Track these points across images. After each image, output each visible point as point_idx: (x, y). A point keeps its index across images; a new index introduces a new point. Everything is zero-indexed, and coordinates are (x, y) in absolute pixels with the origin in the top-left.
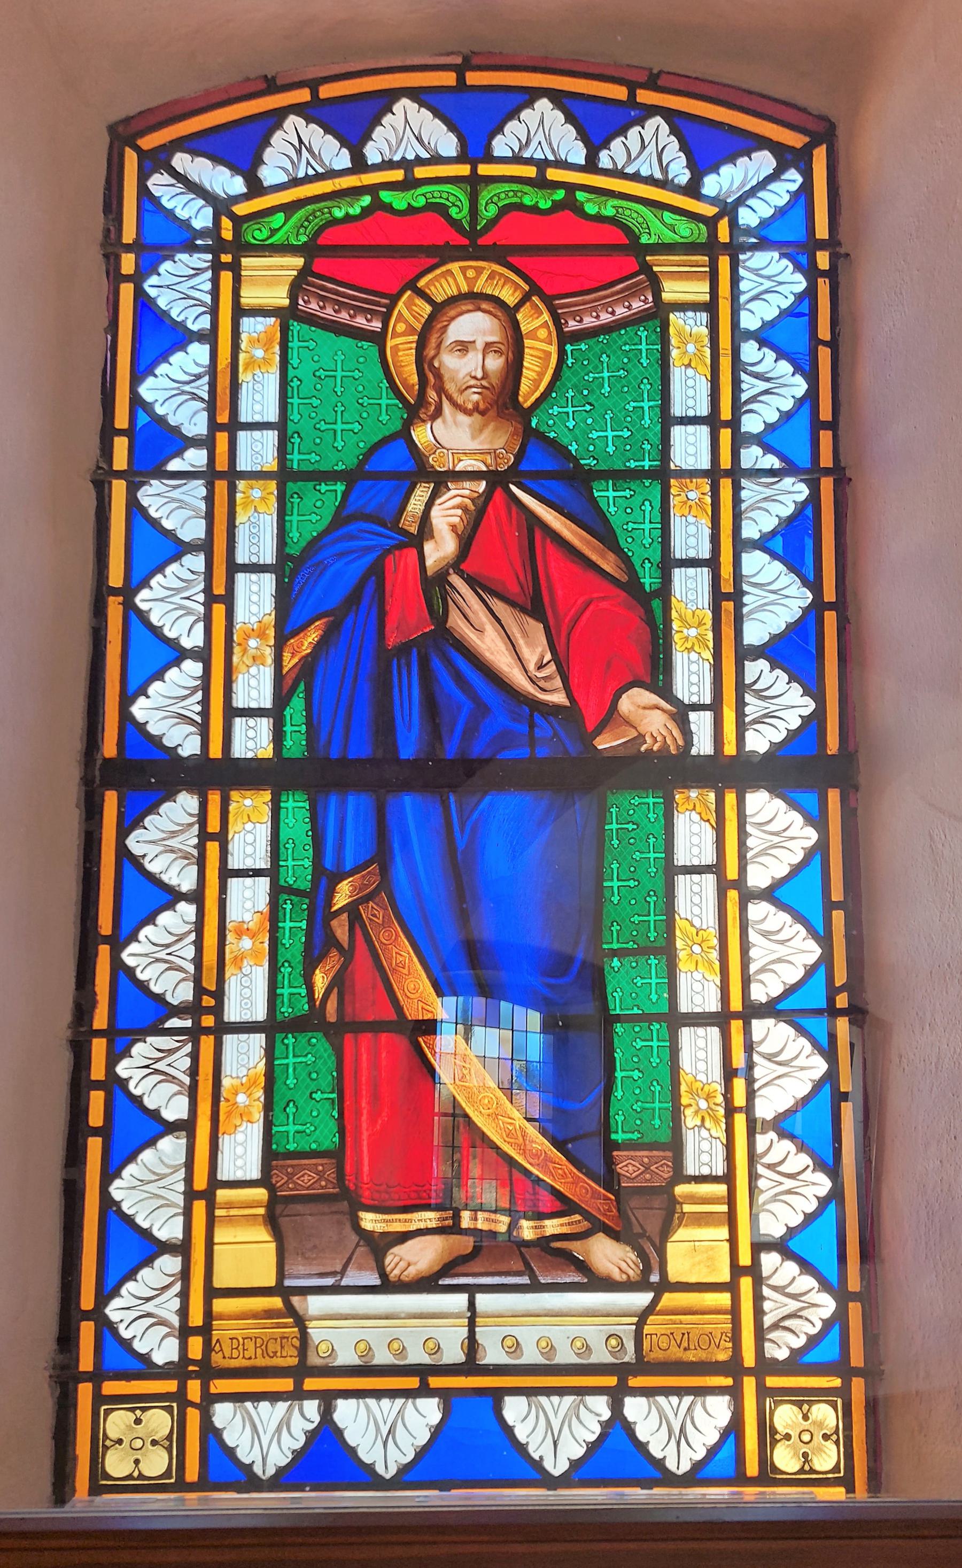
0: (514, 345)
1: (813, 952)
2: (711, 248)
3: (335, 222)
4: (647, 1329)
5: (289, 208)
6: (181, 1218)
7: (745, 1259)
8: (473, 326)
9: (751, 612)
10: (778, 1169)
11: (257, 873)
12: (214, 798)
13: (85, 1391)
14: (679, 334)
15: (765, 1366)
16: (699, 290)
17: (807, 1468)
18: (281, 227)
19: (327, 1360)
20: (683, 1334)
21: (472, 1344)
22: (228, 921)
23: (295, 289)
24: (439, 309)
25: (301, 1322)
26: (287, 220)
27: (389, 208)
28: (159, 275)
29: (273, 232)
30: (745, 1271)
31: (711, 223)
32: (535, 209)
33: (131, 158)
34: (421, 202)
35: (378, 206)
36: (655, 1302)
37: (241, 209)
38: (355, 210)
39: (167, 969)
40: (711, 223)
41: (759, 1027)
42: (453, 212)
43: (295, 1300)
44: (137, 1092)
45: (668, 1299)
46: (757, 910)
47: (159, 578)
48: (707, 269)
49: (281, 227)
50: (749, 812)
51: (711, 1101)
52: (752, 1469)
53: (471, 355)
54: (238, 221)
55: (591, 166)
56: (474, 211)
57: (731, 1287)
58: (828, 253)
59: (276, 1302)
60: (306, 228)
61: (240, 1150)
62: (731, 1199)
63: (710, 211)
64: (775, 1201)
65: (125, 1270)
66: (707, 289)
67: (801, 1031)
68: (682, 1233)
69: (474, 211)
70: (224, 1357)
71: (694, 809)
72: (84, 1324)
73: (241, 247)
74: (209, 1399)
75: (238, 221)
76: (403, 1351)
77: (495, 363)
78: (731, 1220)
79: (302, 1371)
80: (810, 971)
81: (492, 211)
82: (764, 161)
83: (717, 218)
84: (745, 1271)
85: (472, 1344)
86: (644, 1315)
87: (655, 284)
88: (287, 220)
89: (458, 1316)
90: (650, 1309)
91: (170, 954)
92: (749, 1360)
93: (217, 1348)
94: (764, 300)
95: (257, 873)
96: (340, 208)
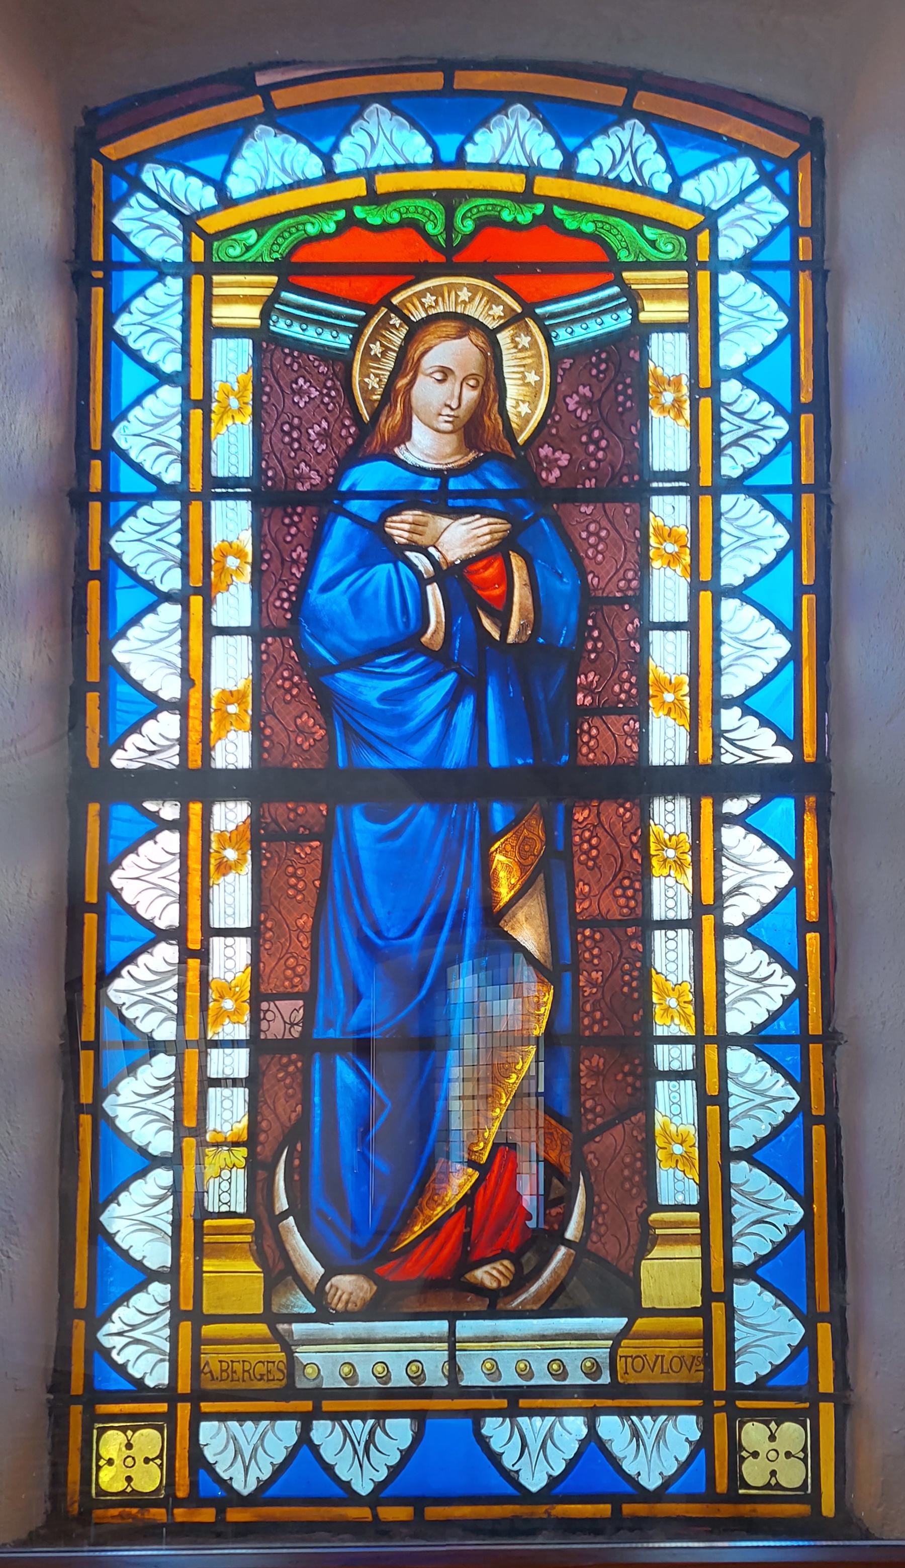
0: (492, 378)
1: (784, 874)
2: (691, 265)
3: (309, 240)
4: (621, 1352)
5: (261, 224)
6: (177, 906)
7: (718, 1286)
8: (450, 352)
9: (727, 332)
10: (746, 416)
11: (235, 1082)
12: (195, 761)
13: (76, 1410)
14: (658, 841)
15: (735, 1391)
16: (677, 310)
17: (773, 1482)
18: (255, 244)
19: (317, 1381)
20: (657, 1357)
21: (453, 1369)
22: (212, 687)
23: (268, 309)
24: (415, 330)
25: (287, 1345)
26: (260, 236)
27: (363, 223)
28: (131, 313)
29: (248, 248)
30: (718, 1297)
31: (691, 235)
32: (514, 225)
33: (97, 168)
34: (395, 218)
35: (351, 222)
36: (628, 1326)
37: (210, 224)
38: (330, 228)
39: (152, 1010)
40: (691, 235)
41: (727, 501)
42: (430, 228)
43: (281, 1327)
44: (120, 1360)
45: (642, 1324)
46: (729, 606)
47: (131, 857)
48: (687, 286)
49: (255, 244)
50: (722, 293)
51: (682, 999)
52: (722, 1485)
53: (447, 385)
54: (209, 239)
55: (568, 170)
56: (449, 227)
57: (704, 1312)
58: (809, 265)
59: (261, 1329)
60: (280, 245)
61: (227, 1104)
62: (704, 1223)
63: (688, 220)
64: (746, 999)
65: (136, 288)
66: (686, 307)
67: (766, 505)
68: (657, 1252)
69: (449, 227)
70: (213, 1379)
71: (671, 836)
72: (87, 916)
73: (210, 268)
74: (197, 1418)
75: (209, 239)
76: (388, 1377)
77: (470, 395)
78: (704, 1241)
79: (290, 1392)
80: (783, 893)
81: (469, 226)
82: (744, 170)
83: (698, 229)
84: (718, 1297)
85: (453, 1369)
86: (618, 1338)
87: (633, 299)
88: (260, 236)
89: (439, 1340)
90: (625, 1332)
91: (154, 994)
92: (719, 1384)
93: (207, 1370)
94: (745, 894)
95: (235, 1082)
96: (313, 224)
